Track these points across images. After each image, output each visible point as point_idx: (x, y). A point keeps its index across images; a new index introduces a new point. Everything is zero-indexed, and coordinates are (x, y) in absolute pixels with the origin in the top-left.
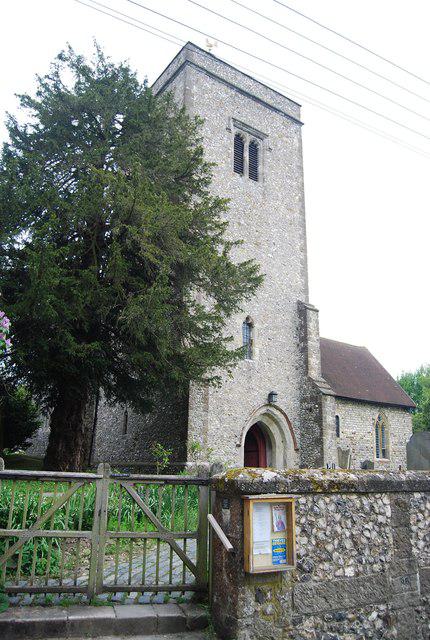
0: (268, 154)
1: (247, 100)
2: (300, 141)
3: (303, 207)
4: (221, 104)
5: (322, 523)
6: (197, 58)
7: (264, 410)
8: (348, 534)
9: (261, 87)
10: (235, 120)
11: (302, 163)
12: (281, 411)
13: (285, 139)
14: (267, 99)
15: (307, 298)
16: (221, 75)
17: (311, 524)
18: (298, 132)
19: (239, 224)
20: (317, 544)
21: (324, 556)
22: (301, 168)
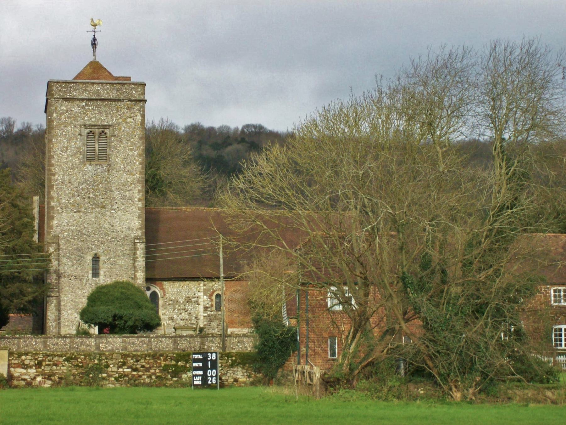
0: (113, 139)
13: (129, 120)
18: (143, 107)
19: (89, 197)
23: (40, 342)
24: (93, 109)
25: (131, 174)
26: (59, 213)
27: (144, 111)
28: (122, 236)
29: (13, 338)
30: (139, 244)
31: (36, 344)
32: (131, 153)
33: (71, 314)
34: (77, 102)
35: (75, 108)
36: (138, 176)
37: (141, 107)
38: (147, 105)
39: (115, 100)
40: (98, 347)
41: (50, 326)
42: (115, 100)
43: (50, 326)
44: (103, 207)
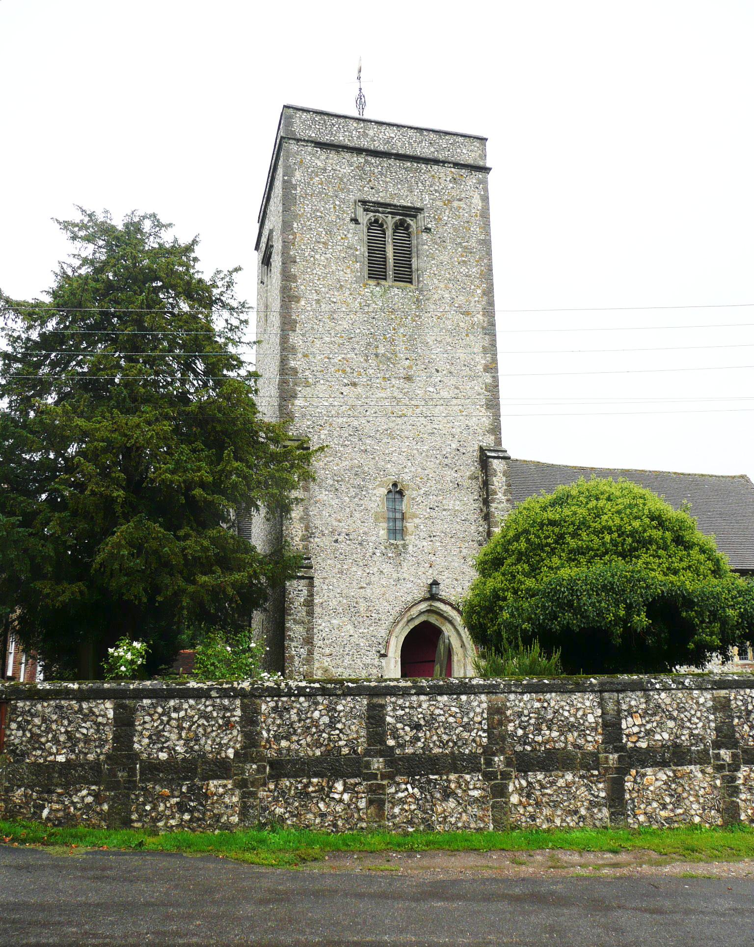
0: (425, 236)
1: (386, 162)
2: (485, 199)
3: (491, 303)
4: (342, 185)
5: (37, 721)
6: (299, 128)
7: (423, 606)
8: (63, 730)
9: (411, 133)
10: (364, 202)
11: (488, 234)
12: (451, 605)
13: (456, 204)
14: (424, 150)
15: (498, 442)
16: (341, 138)
17: (28, 722)
18: (484, 182)
19: (377, 355)
20: (31, 737)
21: (37, 745)
22: (486, 243)
23: (350, 714)
24: (381, 174)
25: (467, 313)
26: (307, 385)
27: (486, 190)
28: (454, 446)
29: (224, 693)
30: (495, 461)
31: (332, 725)
32: (464, 270)
33: (340, 628)
34: (348, 155)
35: (344, 166)
36: (481, 317)
37: (480, 182)
38: (491, 177)
39: (427, 161)
40: (611, 728)
41: (293, 657)
42: (427, 161)
43: (293, 657)
44: (408, 379)
